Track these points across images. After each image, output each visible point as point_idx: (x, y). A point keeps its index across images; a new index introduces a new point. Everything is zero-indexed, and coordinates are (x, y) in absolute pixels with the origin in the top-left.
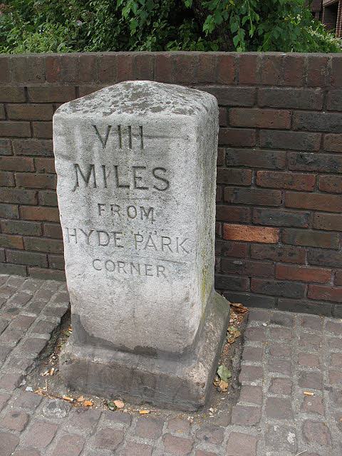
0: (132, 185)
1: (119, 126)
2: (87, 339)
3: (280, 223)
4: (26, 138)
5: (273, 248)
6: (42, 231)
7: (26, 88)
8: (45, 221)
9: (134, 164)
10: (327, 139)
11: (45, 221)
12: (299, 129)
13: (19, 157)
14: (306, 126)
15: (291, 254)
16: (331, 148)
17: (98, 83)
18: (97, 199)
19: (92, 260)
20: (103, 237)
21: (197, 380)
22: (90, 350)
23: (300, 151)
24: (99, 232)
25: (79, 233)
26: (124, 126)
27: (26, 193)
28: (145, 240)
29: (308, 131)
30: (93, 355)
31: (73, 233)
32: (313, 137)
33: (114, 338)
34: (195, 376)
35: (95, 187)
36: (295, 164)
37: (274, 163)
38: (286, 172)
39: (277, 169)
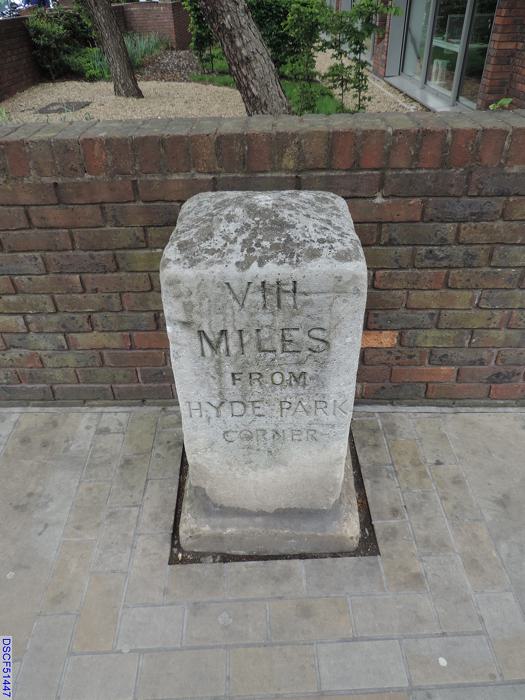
0: (279, 348)
1: (263, 283)
2: (210, 507)
3: (399, 326)
4: (66, 250)
5: (389, 353)
6: (102, 360)
7: (56, 184)
8: (105, 348)
9: (283, 325)
10: (465, 229)
11: (105, 348)
12: (432, 220)
13: (59, 276)
14: (440, 215)
15: (411, 357)
16: (467, 240)
17: (166, 175)
18: (228, 368)
19: (222, 432)
20: (238, 408)
21: (351, 535)
22: (219, 521)
23: (430, 245)
24: (232, 403)
25: (206, 406)
26: (272, 281)
27: (73, 318)
28: (294, 406)
29: (442, 222)
30: (224, 527)
31: (197, 406)
32: (451, 227)
33: (252, 504)
34: (348, 531)
35: (228, 355)
36: (422, 261)
37: (396, 261)
38: (410, 271)
39: (401, 268)
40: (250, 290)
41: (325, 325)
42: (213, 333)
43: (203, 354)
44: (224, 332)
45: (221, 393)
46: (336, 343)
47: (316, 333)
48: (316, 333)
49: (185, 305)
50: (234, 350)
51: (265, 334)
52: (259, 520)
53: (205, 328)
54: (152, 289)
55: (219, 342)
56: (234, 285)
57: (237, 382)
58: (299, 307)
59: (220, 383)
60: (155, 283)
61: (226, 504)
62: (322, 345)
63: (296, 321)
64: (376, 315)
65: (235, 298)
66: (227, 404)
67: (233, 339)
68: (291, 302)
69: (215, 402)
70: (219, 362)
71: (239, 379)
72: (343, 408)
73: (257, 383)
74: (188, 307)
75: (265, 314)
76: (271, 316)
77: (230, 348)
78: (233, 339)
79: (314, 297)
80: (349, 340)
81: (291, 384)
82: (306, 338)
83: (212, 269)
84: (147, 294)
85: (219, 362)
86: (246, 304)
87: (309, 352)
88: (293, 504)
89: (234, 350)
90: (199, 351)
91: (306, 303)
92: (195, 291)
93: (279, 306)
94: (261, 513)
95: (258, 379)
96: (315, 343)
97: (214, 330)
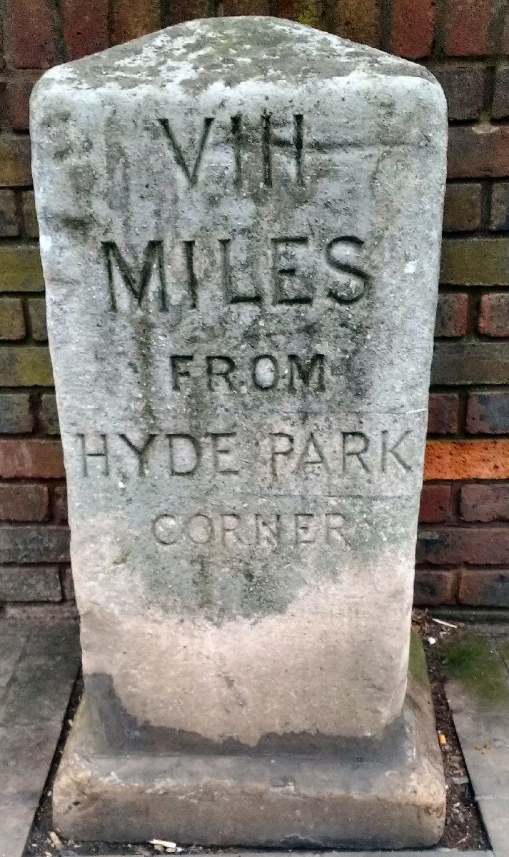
20: (184, 451)
25: (117, 445)
34: (421, 790)
40: (210, 139)
41: (362, 231)
42: (132, 248)
43: (114, 307)
44: (155, 246)
45: (148, 411)
46: (386, 279)
47: (344, 252)
48: (344, 252)
49: (74, 173)
50: (176, 295)
51: (238, 252)
52: (226, 762)
53: (117, 237)
54: (63, 601)
55: (146, 274)
56: (176, 123)
57: (182, 380)
58: (308, 180)
59: (146, 381)
60: (35, 322)
61: (155, 717)
62: (355, 283)
63: (301, 220)
64: (484, 400)
65: (180, 161)
66: (161, 441)
67: (176, 257)
68: (292, 169)
69: (136, 437)
70: (145, 327)
71: (187, 374)
72: (403, 450)
73: (222, 381)
74: (81, 183)
75: (239, 197)
76: (250, 207)
77: (169, 290)
78: (176, 257)
79: (338, 157)
80: (410, 268)
81: (291, 388)
82: (325, 267)
83: (135, 90)
84: (16, 350)
85: (145, 327)
86: (202, 176)
87: (329, 303)
88: (299, 723)
89: (176, 295)
90: (102, 296)
91: (323, 172)
92: (100, 141)
93: (268, 182)
94: (231, 747)
95: (225, 375)
96: (342, 278)
97: (135, 241)
